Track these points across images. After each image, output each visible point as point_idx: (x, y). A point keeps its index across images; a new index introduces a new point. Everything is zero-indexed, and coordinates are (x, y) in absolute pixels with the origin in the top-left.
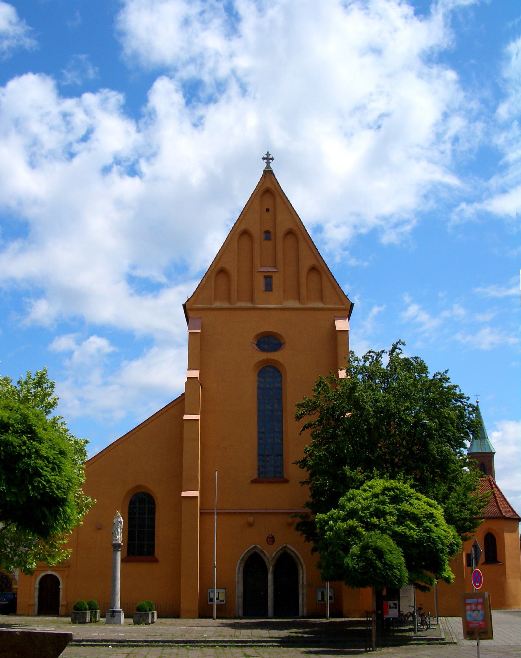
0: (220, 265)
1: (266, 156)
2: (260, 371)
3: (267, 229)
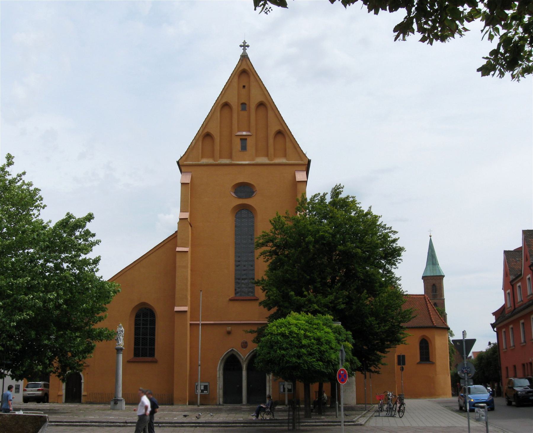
0: (206, 131)
1: (243, 44)
2: (237, 213)
3: (243, 101)
